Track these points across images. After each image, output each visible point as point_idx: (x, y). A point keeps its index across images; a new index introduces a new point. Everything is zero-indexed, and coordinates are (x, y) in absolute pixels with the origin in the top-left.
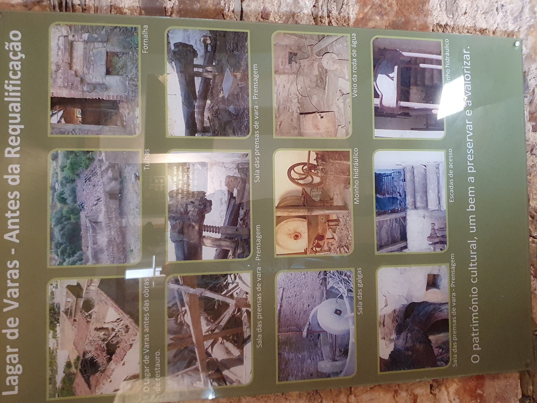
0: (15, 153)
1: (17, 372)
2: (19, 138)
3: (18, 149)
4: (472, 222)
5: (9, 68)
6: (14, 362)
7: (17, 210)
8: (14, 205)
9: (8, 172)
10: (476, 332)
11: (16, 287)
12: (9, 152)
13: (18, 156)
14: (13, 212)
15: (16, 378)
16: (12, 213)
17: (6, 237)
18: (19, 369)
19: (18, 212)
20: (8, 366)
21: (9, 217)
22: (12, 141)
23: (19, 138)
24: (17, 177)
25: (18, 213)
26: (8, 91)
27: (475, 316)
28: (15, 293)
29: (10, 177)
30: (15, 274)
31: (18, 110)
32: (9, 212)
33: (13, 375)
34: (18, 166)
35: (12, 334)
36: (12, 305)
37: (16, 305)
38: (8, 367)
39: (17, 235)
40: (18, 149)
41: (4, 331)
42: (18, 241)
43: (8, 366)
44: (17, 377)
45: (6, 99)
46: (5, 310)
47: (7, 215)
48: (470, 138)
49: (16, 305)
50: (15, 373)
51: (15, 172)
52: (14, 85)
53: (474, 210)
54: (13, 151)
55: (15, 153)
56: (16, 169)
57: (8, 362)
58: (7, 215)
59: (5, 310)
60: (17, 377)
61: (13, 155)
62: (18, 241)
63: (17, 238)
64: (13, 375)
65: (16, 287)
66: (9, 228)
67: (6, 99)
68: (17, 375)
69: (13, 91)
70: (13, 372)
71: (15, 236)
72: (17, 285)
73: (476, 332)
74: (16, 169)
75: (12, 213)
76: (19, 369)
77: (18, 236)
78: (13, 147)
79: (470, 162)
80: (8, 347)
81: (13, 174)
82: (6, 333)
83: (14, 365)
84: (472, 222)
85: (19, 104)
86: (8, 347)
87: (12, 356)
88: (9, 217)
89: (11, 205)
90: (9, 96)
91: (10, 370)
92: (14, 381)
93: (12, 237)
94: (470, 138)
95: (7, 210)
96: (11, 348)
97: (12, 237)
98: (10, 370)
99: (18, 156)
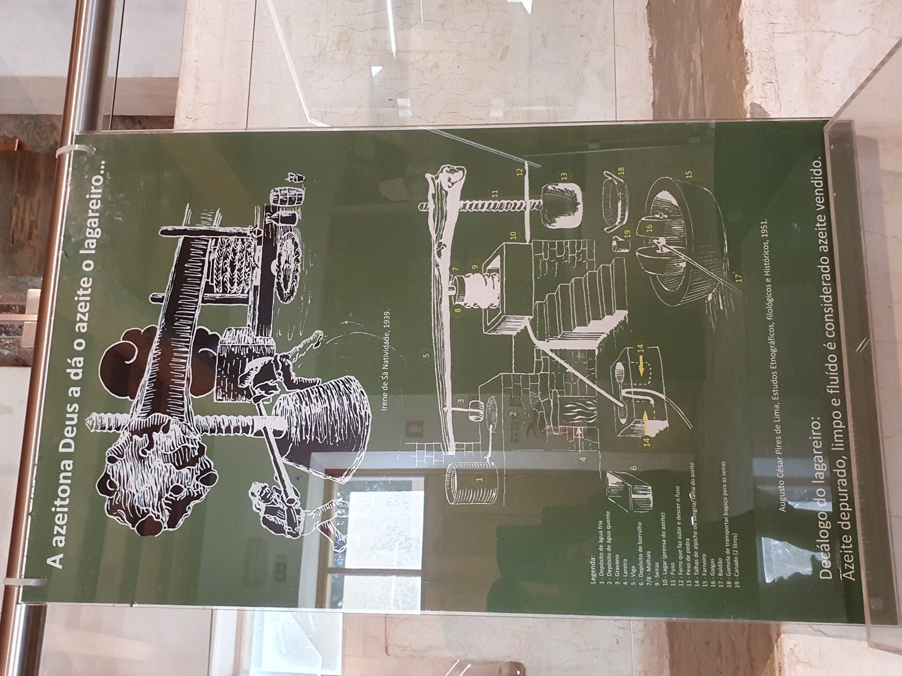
1: (96, 236)
2: (66, 516)
4: (838, 438)
6: (93, 225)
14: (85, 289)
15: (94, 241)
17: (49, 561)
22: (59, 519)
23: (66, 516)
24: (80, 371)
27: (837, 433)
29: (73, 371)
30: (77, 392)
31: (94, 246)
33: (92, 238)
34: (82, 359)
35: (76, 374)
38: (88, 230)
41: (68, 371)
42: (60, 567)
47: (56, 503)
51: (68, 469)
52: (834, 389)
56: (80, 362)
58: (56, 503)
62: (60, 567)
64: (92, 238)
70: (92, 235)
71: (58, 561)
72: (98, 214)
74: (80, 362)
81: (76, 367)
84: (838, 438)
87: (93, 220)
89: (59, 519)
91: (90, 233)
92: (61, 542)
93: (55, 561)
97: (55, 561)
98: (90, 233)
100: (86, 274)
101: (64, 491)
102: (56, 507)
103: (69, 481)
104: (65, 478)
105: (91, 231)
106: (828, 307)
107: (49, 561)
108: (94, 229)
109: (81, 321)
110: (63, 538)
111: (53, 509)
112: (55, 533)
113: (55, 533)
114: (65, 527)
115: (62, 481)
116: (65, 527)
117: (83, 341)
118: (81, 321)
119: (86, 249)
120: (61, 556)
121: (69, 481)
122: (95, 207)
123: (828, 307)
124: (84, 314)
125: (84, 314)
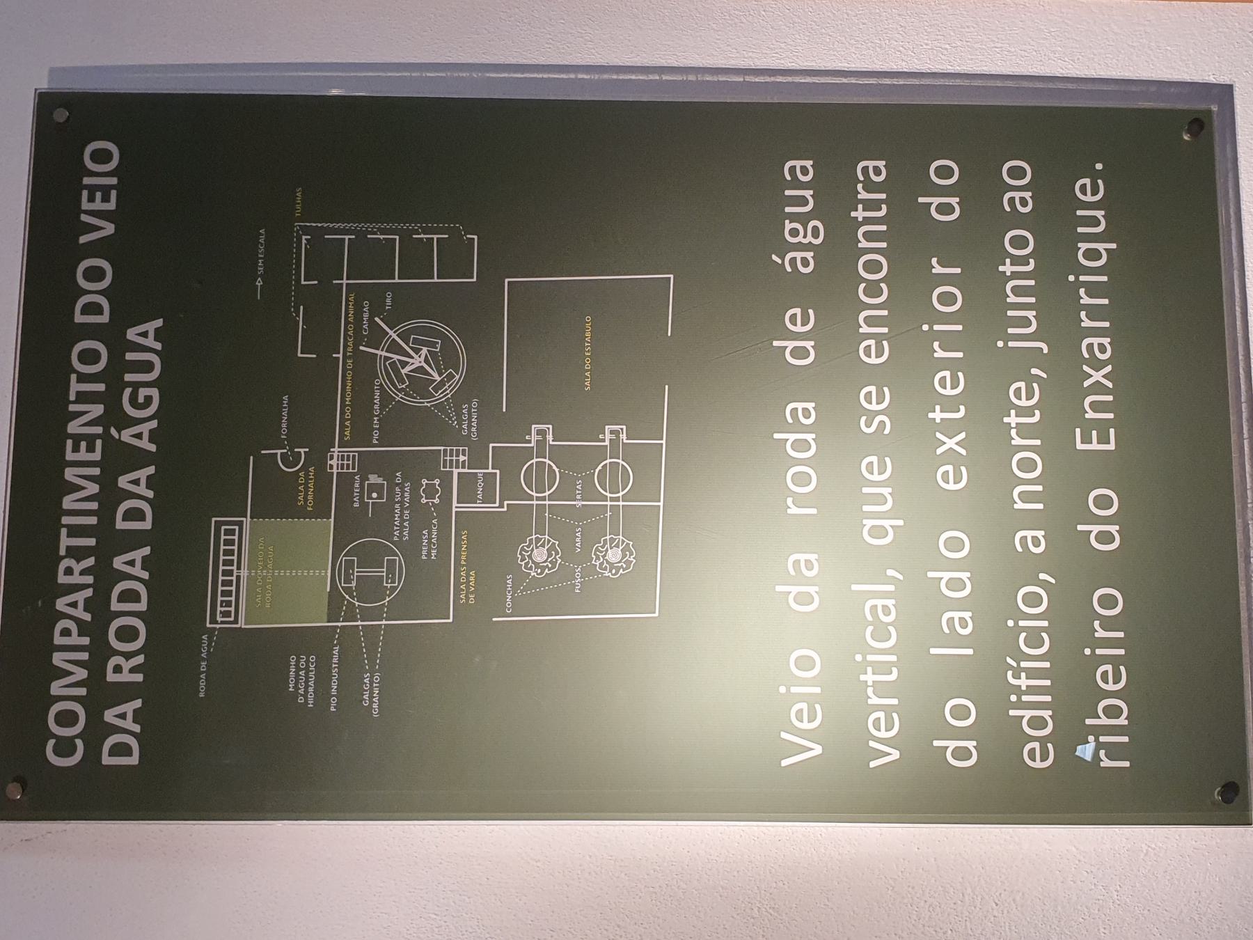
0: (132, 671)
3: (140, 659)
10: (871, 205)
11: (885, 595)
12: (118, 669)
13: (139, 678)
15: (809, 255)
26: (1017, 690)
33: (800, 247)
36: (102, 228)
37: (109, 229)
40: (140, 659)
46: (83, 239)
49: (109, 229)
50: (805, 241)
53: (134, 760)
54: (127, 665)
55: (132, 671)
59: (83, 239)
61: (125, 677)
64: (800, 247)
65: (885, 595)
66: (1030, 194)
69: (1031, 690)
73: (871, 205)
78: (128, 656)
98: (794, 232)
99: (139, 678)
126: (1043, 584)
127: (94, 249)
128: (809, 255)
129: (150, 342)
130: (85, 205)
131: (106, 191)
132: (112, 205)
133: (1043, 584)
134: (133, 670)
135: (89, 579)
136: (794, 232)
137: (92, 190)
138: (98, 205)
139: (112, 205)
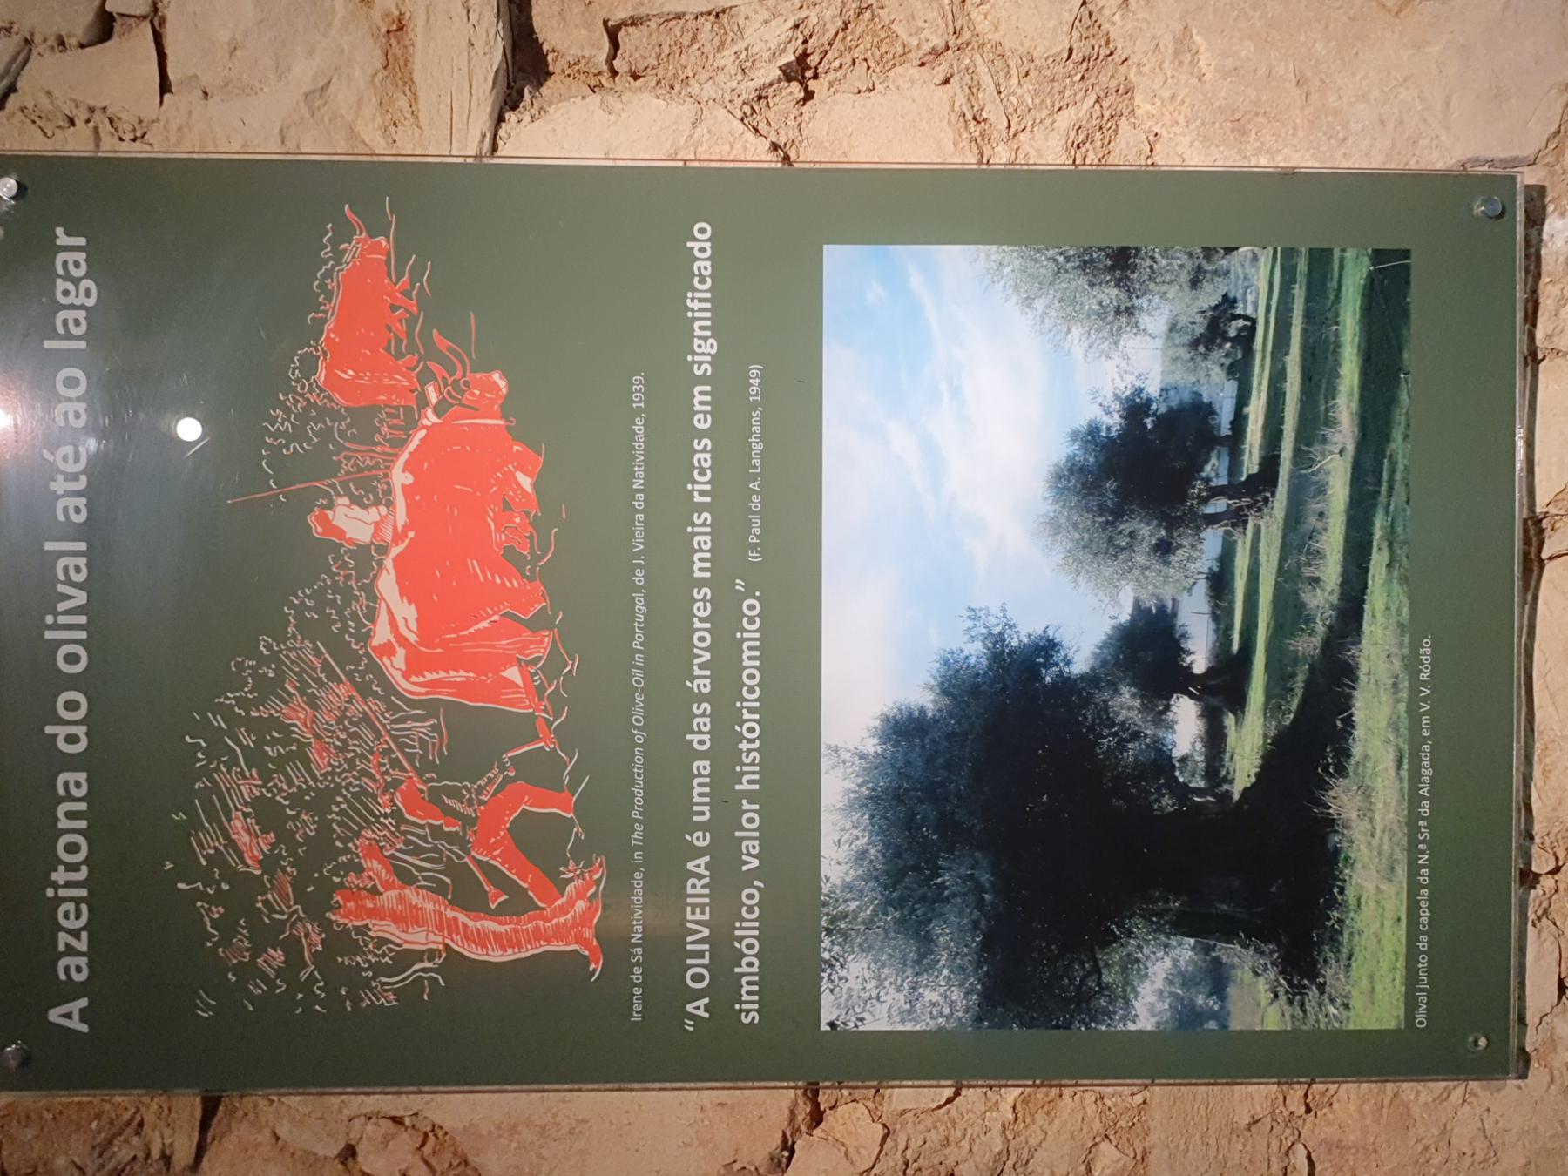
2: (84, 907)
5: (56, 576)
7: (82, 863)
8: (72, 915)
9: (55, 330)
15: (81, 315)
16: (67, 870)
17: (54, 1015)
18: (88, 293)
19: (84, 868)
20: (59, 281)
21: (60, 492)
22: (66, 915)
23: (84, 907)
25: (82, 483)
28: (77, 265)
31: (83, 791)
32: (61, 868)
33: (72, 307)
38: (61, 285)
39: (82, 1011)
42: (84, 1028)
43: (59, 281)
44: (84, 313)
45: (49, 635)
47: (54, 876)
48: (701, 666)
50: (77, 302)
54: (699, 884)
57: (61, 272)
58: (54, 876)
60: (84, 313)
62: (84, 1028)
63: (82, 1020)
64: (72, 307)
67: (49, 635)
68: (82, 307)
71: (76, 1016)
75: (67, 870)
76: (88, 293)
77: (84, 1015)
79: (701, 620)
80: (59, 231)
81: (700, 732)
82: (56, 736)
83: (76, 282)
85: (84, 560)
86: (59, 231)
88: (60, 492)
89: (66, 915)
90: (56, 627)
92: (79, 969)
93: (68, 1016)
94: (701, 666)
95: (55, 862)
96: (68, 234)
97: (68, 1016)
98: (66, 293)
100: (73, 682)
101: (72, 848)
102: (56, 886)
103: (83, 824)
104: (70, 815)
105: (70, 286)
106: (700, 363)
107: (54, 1015)
108: (76, 282)
109: (71, 951)
110: (83, 961)
111: (50, 892)
112: (61, 948)
113: (61, 948)
114: (84, 935)
115: (64, 823)
116: (84, 935)
117: (80, 697)
118: (71, 951)
119: (61, 337)
120: (84, 1002)
121: (83, 824)
122: (703, 614)
123: (700, 363)
124: (75, 934)
125: (75, 934)
126: (758, 888)
127: (699, 994)
128: (81, 315)
129: (702, 871)
130: (689, 917)
131: (702, 907)
132: (706, 917)
133: (758, 888)
134: (703, 887)
135: (707, 891)
136: (66, 293)
137: (694, 906)
138: (698, 917)
139: (706, 917)
